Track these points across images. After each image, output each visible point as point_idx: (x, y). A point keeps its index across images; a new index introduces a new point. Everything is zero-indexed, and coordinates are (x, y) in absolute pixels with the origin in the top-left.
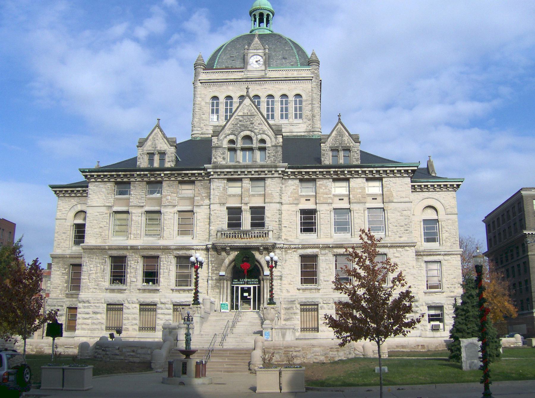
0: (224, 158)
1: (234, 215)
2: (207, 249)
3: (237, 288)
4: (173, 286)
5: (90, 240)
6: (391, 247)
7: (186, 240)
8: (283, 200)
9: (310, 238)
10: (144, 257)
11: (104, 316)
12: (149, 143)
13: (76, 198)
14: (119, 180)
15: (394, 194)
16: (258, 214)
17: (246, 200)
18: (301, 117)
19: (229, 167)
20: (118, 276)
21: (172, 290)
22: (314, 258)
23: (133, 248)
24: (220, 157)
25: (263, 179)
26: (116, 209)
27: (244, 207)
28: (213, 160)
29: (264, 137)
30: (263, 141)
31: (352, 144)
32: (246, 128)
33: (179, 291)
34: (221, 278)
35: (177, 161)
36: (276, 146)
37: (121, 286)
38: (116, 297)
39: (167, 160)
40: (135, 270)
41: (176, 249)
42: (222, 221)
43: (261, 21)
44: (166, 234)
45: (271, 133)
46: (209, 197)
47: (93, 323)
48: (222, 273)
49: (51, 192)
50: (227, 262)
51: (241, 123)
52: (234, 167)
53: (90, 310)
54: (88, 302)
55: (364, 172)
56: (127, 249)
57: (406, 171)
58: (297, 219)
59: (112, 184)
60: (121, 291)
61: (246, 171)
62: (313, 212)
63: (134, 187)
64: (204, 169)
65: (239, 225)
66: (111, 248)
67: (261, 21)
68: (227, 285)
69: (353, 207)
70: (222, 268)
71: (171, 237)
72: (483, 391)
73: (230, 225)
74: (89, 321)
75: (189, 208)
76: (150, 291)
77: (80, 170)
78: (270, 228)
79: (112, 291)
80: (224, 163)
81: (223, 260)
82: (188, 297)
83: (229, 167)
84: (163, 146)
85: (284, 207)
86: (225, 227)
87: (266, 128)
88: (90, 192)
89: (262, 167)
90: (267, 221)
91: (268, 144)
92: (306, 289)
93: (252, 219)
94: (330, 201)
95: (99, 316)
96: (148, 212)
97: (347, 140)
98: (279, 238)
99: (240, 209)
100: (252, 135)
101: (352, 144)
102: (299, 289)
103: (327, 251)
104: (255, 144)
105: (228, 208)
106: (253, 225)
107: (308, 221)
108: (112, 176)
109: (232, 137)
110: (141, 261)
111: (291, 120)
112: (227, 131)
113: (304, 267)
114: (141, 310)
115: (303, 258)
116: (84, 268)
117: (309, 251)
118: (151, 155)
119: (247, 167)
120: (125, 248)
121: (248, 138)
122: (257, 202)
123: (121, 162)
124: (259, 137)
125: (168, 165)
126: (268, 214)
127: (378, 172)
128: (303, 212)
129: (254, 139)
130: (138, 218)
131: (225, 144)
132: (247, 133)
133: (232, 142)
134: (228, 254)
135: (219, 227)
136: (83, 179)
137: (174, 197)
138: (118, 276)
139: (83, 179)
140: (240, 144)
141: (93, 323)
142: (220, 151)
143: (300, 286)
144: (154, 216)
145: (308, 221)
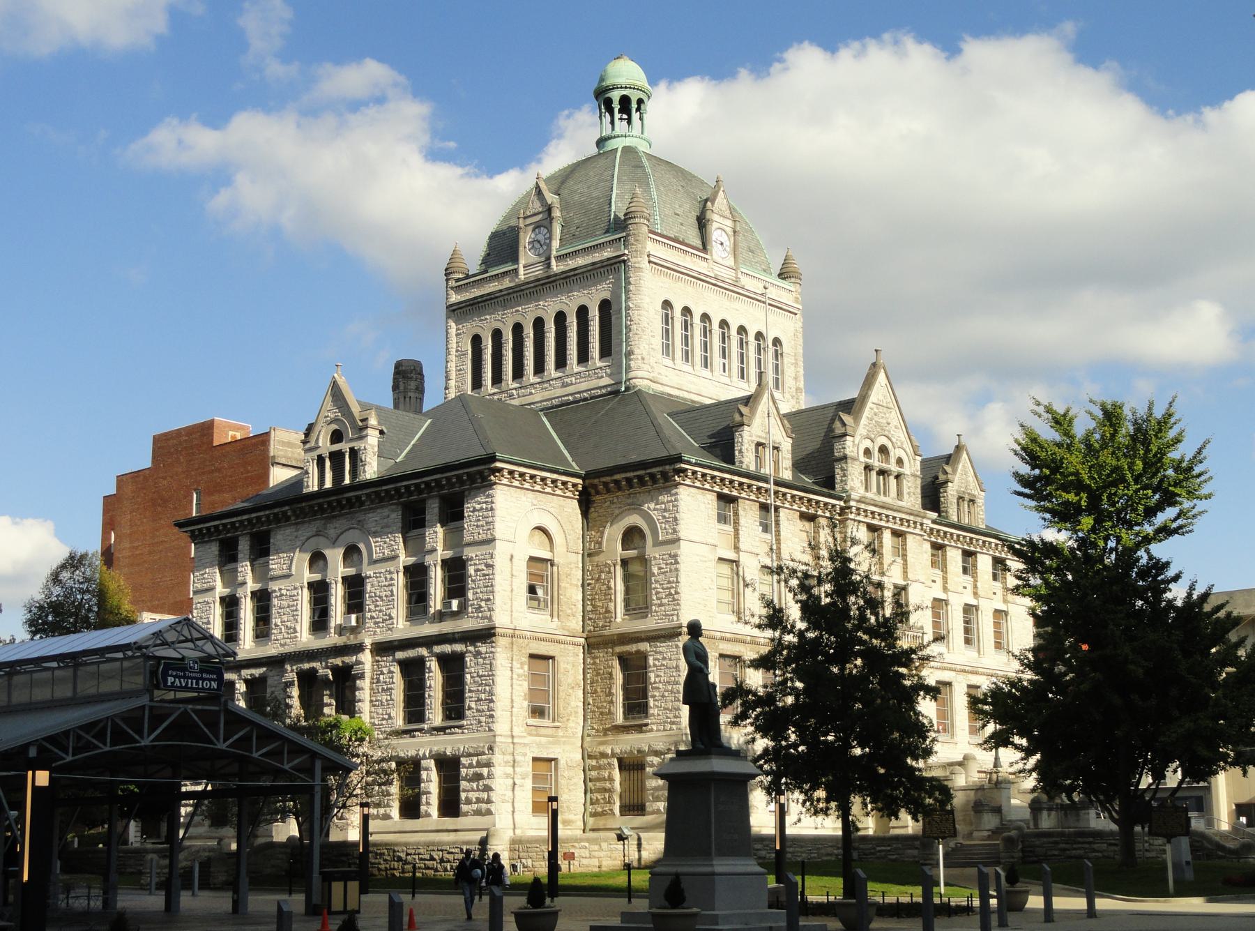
13: (530, 494)
51: (876, 418)
56: (744, 642)
59: (713, 497)
63: (745, 510)
100: (890, 446)
109: (868, 444)
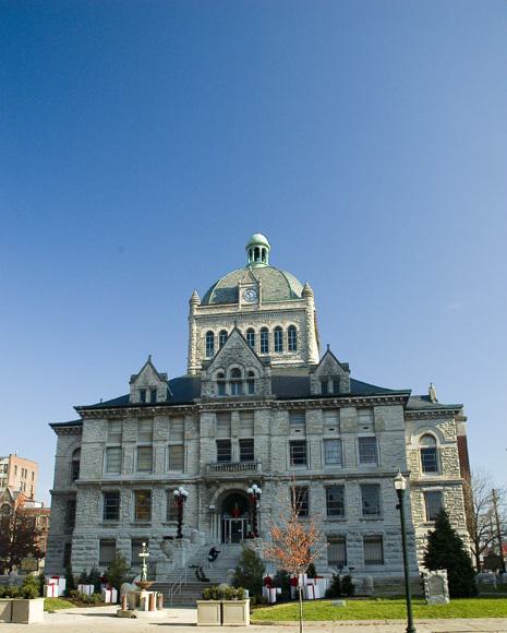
0: (213, 392)
1: (224, 446)
2: (197, 483)
3: (228, 522)
4: (132, 521)
5: (84, 477)
6: (383, 477)
7: (176, 474)
8: (271, 434)
9: (301, 470)
10: (135, 492)
11: (98, 552)
12: (140, 379)
14: (112, 416)
15: (386, 423)
16: (247, 446)
17: (234, 432)
18: (295, 348)
19: (218, 400)
20: (111, 512)
21: (361, 520)
22: (305, 489)
23: (126, 484)
24: (210, 391)
25: (252, 411)
26: (108, 445)
27: (233, 440)
28: (203, 394)
29: (253, 369)
30: (251, 374)
31: (342, 372)
32: (235, 361)
33: (169, 525)
34: (211, 512)
35: (169, 396)
36: (264, 378)
37: (113, 522)
38: (109, 532)
39: (158, 394)
40: (353, 498)
41: (167, 484)
42: (210, 454)
43: (257, 255)
44: (157, 468)
45: (259, 365)
46: (198, 430)
47: (87, 559)
48: (212, 507)
49: (52, 432)
50: (216, 495)
52: (223, 400)
53: (84, 546)
54: (82, 537)
55: (354, 401)
57: (398, 399)
58: (286, 451)
60: (113, 526)
61: (234, 403)
62: (304, 443)
64: (193, 403)
65: (229, 458)
66: (104, 484)
67: (257, 255)
68: (217, 520)
69: (343, 436)
70: (213, 502)
71: (162, 472)
72: (406, 626)
73: (219, 459)
74: (82, 557)
75: (148, 444)
76: (142, 526)
77: (75, 408)
78: (259, 460)
79: (105, 526)
80: (212, 396)
81: (213, 494)
82: (173, 531)
83: (218, 400)
84: (153, 381)
85: (274, 439)
86: (215, 459)
87: (254, 360)
88: (84, 428)
89: (251, 399)
90: (256, 453)
91: (257, 376)
92: (368, 520)
93: (242, 451)
94: (320, 431)
95: (92, 552)
96: (139, 447)
97: (336, 369)
98: (268, 470)
99: (229, 441)
100: (241, 367)
101: (342, 372)
102: (361, 520)
103: (317, 482)
104: (243, 377)
105: (217, 441)
106: (242, 458)
107: (299, 453)
108: (104, 412)
110: (133, 495)
111: (285, 353)
112: (215, 365)
113: (329, 498)
114: (133, 545)
115: (328, 488)
116: (78, 505)
117: (300, 483)
118: (143, 393)
119: (236, 399)
120: (117, 483)
121: (236, 372)
122: (246, 434)
123: (373, 386)
124: (248, 369)
125: (159, 400)
126: (256, 446)
127: (368, 400)
128: (292, 443)
129: (243, 371)
130: (130, 452)
131: (214, 378)
132: (236, 366)
133: (221, 375)
134: (218, 487)
135: (209, 460)
136: (77, 417)
137: (164, 433)
138: (111, 512)
139: (77, 417)
140: (228, 377)
141: (87, 559)
142: (209, 384)
143: (362, 517)
144: (146, 452)
145: (299, 453)
